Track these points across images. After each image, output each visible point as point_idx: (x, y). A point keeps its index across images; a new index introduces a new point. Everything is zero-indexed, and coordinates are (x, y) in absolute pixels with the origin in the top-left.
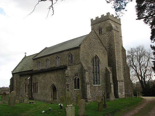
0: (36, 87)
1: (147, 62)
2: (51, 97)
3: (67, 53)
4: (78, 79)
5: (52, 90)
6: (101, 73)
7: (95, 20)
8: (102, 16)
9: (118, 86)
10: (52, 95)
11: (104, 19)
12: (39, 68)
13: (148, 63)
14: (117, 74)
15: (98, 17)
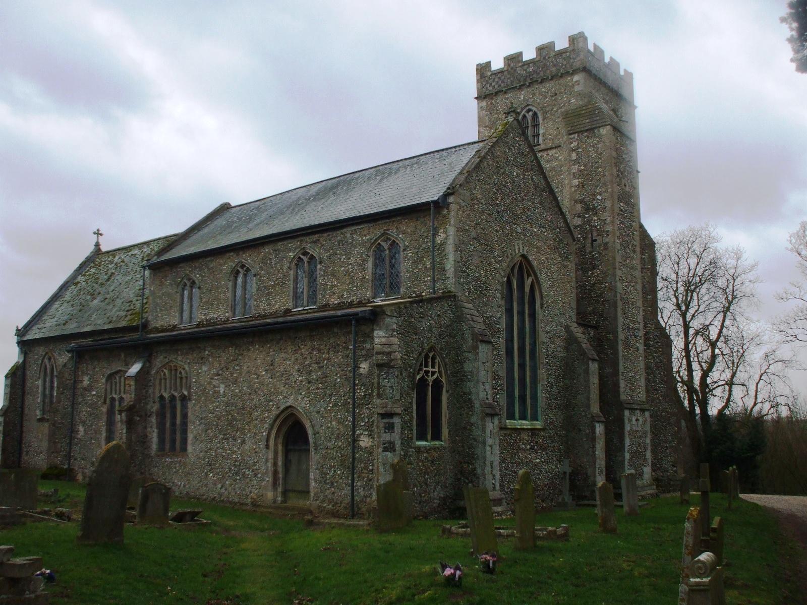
0: (173, 424)
1: (720, 317)
2: (275, 484)
3: (366, 235)
4: (437, 384)
5: (280, 441)
6: (543, 359)
7: (501, 71)
8: (540, 50)
9: (626, 434)
10: (275, 473)
11: (554, 65)
12: (186, 315)
13: (724, 321)
14: (621, 368)
15: (488, 64)
